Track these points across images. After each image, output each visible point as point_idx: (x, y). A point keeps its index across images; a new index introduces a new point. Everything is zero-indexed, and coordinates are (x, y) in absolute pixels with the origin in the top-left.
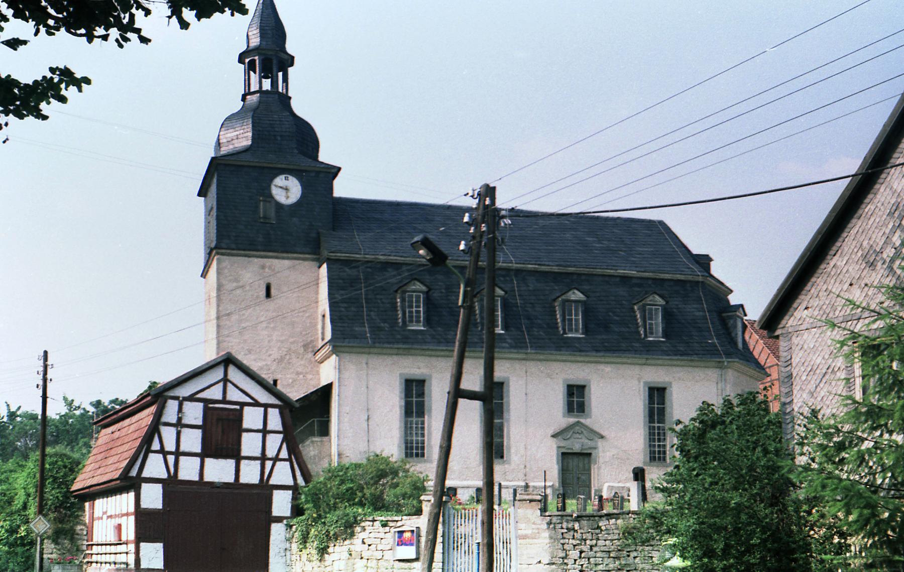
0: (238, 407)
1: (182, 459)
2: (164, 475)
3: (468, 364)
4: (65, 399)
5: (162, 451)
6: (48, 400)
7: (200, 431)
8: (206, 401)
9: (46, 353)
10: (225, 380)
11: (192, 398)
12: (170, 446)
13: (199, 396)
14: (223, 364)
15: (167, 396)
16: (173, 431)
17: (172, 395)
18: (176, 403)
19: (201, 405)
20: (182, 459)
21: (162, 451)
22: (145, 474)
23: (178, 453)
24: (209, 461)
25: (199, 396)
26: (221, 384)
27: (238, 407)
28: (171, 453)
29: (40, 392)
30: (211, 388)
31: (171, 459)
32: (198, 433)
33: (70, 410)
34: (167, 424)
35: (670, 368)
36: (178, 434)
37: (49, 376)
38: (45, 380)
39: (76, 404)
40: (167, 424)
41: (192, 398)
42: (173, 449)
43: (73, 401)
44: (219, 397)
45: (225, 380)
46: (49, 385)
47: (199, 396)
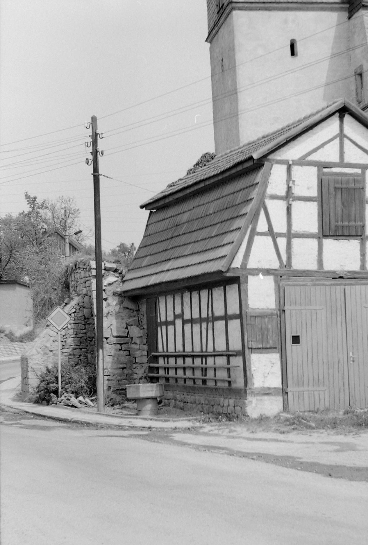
0: (359, 171)
1: (295, 242)
2: (275, 265)
3: (202, 324)
4: (27, 196)
5: (271, 232)
6: (101, 177)
7: (316, 203)
8: (322, 166)
9: (94, 120)
10: (342, 136)
11: (302, 162)
12: (280, 226)
13: (310, 158)
14: (337, 114)
15: (274, 160)
16: (282, 205)
17: (279, 158)
18: (284, 167)
19: (314, 170)
20: (295, 242)
21: (271, 232)
22: (252, 264)
23: (290, 235)
24: (328, 243)
25: (310, 158)
26: (337, 141)
27: (359, 171)
28: (280, 235)
29: (91, 168)
30: (326, 146)
31: (282, 242)
32: (313, 208)
33: (33, 209)
34: (274, 197)
35: (226, 21)
36: (289, 209)
37: (100, 148)
38: (95, 153)
39: (39, 201)
40: (274, 197)
41: (302, 162)
42: (284, 230)
43: (35, 198)
44: (336, 159)
45: (342, 136)
46: (100, 159)
47: (310, 158)
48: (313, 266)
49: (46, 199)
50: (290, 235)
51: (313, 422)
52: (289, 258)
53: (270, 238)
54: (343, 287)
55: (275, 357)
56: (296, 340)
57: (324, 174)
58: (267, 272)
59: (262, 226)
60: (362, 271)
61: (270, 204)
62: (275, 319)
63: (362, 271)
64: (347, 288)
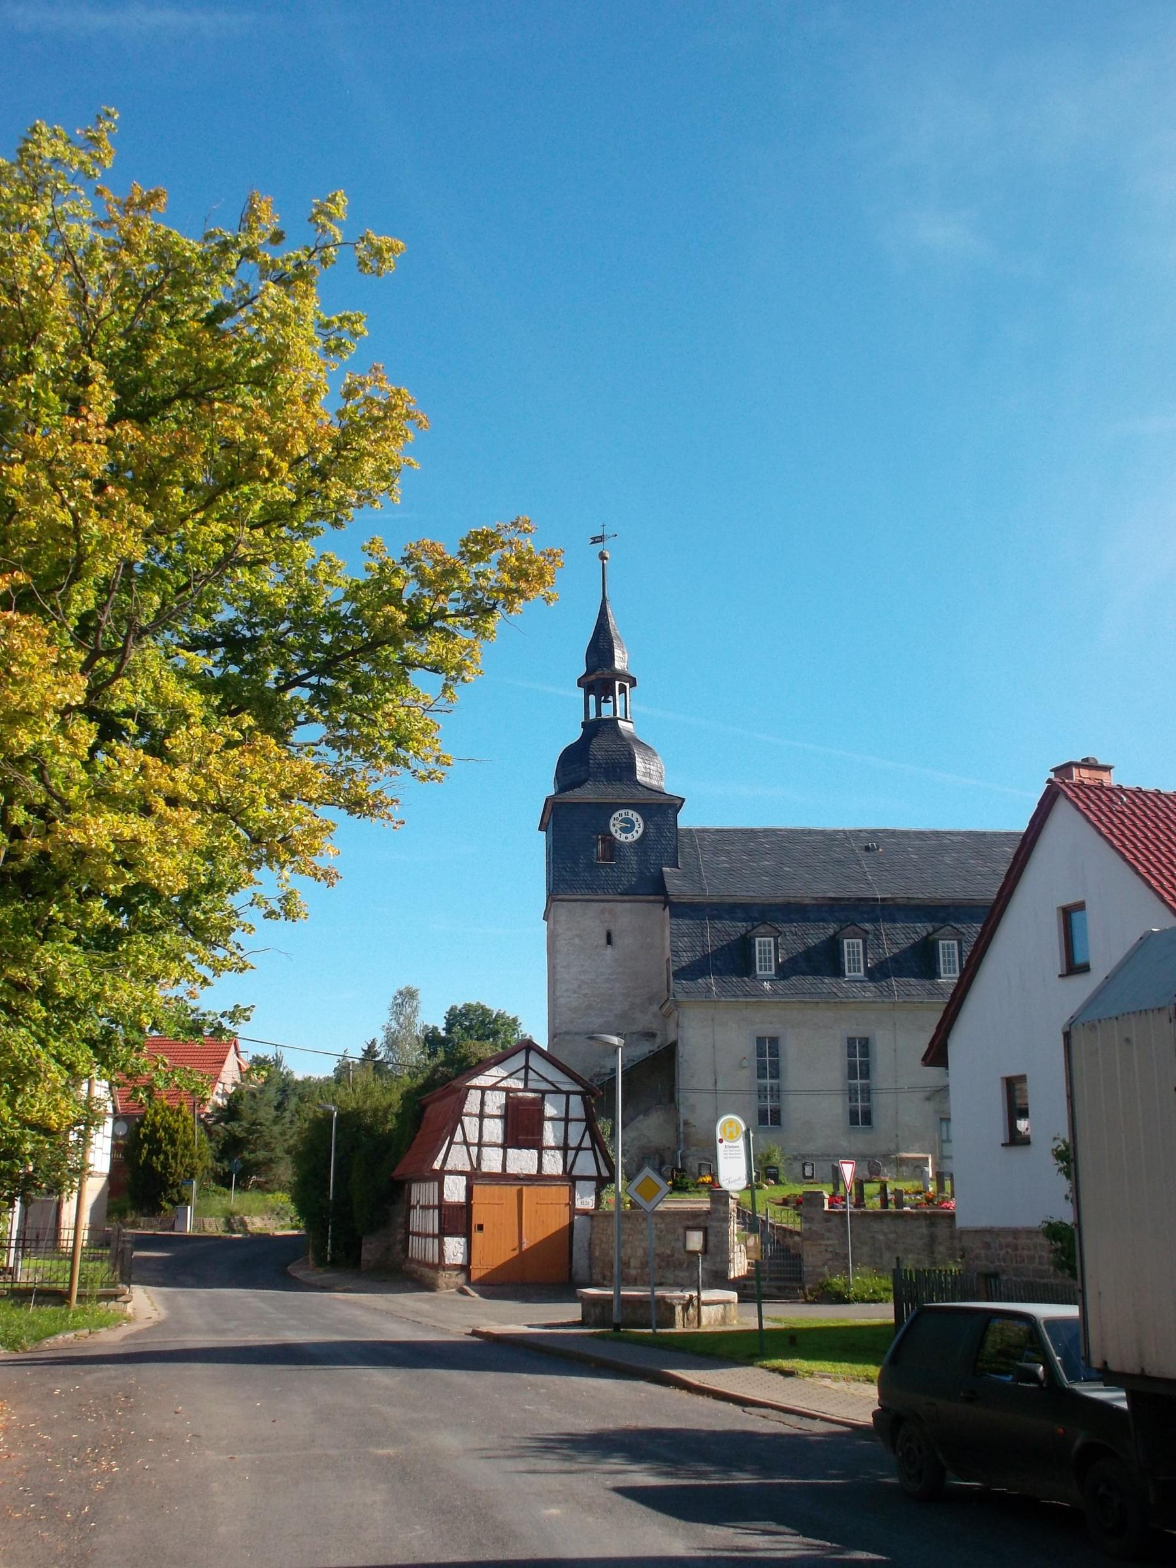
2: (468, 1168)
5: (466, 1143)
8: (507, 1090)
10: (527, 1067)
11: (494, 1088)
12: (473, 1137)
20: (485, 1150)
21: (466, 1143)
23: (480, 1145)
25: (499, 1085)
28: (473, 1145)
31: (474, 1150)
41: (494, 1088)
42: (476, 1141)
45: (527, 1067)
48: (498, 1169)
49: (481, 644)
50: (480, 1145)
51: (34, 1165)
52: (479, 1164)
53: (464, 1147)
54: (519, 1187)
55: (463, 1240)
56: (480, 1227)
57: (510, 1097)
58: (461, 1173)
59: (458, 1137)
60: (228, 1235)
61: (466, 1120)
62: (464, 1211)
63: (228, 1235)
64: (524, 1188)
